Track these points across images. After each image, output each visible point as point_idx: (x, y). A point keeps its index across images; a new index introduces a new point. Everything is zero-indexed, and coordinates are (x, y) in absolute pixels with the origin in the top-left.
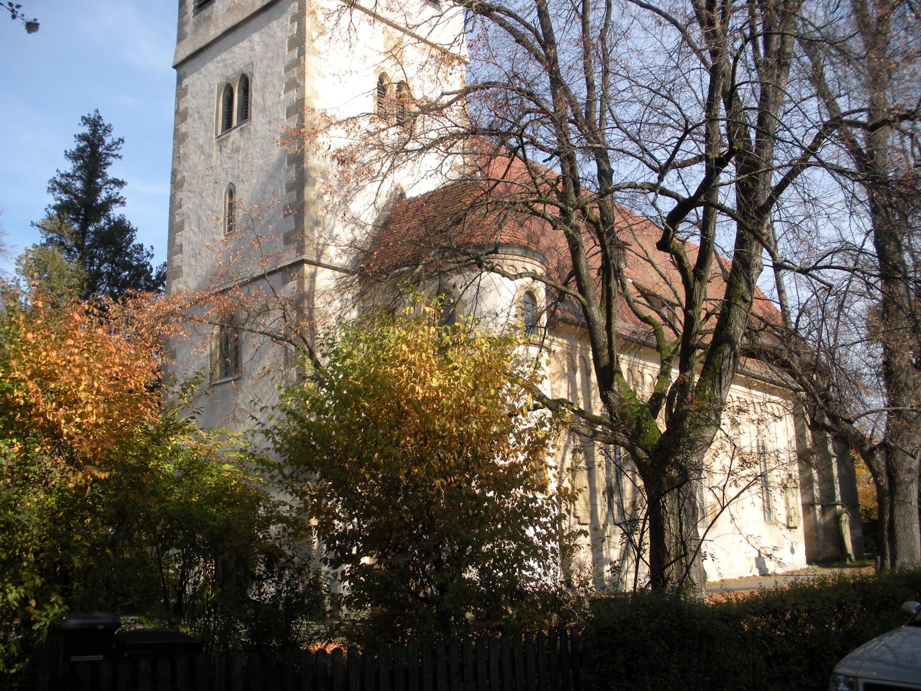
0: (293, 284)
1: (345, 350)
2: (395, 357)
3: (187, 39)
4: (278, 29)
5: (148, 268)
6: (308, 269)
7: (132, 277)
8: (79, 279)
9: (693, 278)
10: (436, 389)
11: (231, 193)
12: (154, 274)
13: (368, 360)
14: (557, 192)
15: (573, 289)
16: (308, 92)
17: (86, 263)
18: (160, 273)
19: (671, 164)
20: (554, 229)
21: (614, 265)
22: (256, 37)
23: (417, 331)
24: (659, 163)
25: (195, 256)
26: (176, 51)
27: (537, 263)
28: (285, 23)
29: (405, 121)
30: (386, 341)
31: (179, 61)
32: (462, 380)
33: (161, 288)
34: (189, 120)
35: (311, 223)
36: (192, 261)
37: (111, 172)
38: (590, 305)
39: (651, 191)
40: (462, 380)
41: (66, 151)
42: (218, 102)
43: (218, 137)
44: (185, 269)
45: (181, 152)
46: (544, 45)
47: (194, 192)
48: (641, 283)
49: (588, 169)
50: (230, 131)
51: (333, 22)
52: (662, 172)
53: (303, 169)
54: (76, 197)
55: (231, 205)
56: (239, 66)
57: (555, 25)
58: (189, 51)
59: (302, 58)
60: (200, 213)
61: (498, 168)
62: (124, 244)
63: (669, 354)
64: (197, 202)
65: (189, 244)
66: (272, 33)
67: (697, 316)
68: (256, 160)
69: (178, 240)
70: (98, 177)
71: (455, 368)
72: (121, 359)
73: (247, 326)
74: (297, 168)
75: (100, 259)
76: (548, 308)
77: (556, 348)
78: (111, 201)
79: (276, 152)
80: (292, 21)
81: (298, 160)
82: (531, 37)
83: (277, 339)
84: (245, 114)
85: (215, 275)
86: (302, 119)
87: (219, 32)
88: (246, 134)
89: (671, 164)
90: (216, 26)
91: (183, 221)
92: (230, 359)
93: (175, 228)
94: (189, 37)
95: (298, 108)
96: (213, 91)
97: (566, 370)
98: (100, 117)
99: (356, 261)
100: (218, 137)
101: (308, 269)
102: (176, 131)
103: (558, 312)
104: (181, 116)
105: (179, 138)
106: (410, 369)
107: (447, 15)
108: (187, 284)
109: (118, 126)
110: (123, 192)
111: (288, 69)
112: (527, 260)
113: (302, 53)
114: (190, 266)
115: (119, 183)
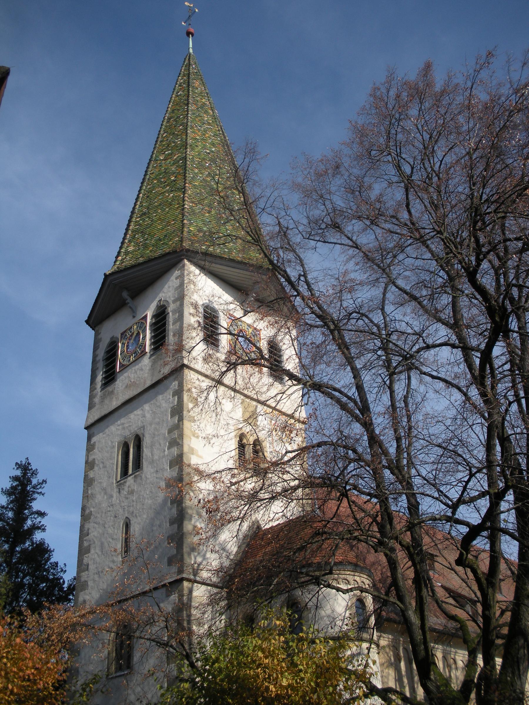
0: (174, 597)
1: (213, 656)
2: (254, 662)
3: (96, 408)
4: (164, 401)
5: (61, 581)
6: (186, 584)
7: (48, 588)
8: (6, 589)
9: (488, 582)
10: (286, 688)
11: (127, 525)
12: (66, 585)
13: (232, 663)
14: (378, 524)
15: (393, 599)
16: (186, 449)
17: (12, 576)
18: (71, 585)
19: (461, 501)
20: (376, 552)
21: (423, 577)
22: (147, 407)
23: (270, 640)
24: (451, 501)
25: (98, 573)
26: (87, 417)
27: (365, 576)
28: (168, 397)
29: (260, 472)
30: (246, 649)
31: (91, 421)
32: (306, 680)
33: (71, 597)
34: (96, 468)
35: (188, 549)
36: (96, 577)
37: (36, 506)
38: (407, 609)
39: (448, 521)
40: (306, 680)
41: (2, 489)
42: (118, 455)
43: (118, 482)
44: (90, 583)
45: (89, 492)
46: (362, 412)
47: (98, 523)
48: (447, 585)
49: (400, 506)
50: (126, 478)
51: (204, 398)
52: (454, 507)
53: (182, 508)
54: (8, 524)
55: (126, 539)
56: (134, 429)
57: (371, 398)
58: (96, 418)
59: (181, 423)
60: (103, 540)
61: (332, 505)
62: (43, 562)
63: (474, 646)
64: (101, 531)
65: (94, 563)
66: (158, 404)
67: (492, 615)
68: (146, 500)
69: (85, 561)
70: (26, 509)
71: (301, 671)
72: (33, 663)
73: (137, 634)
74: (178, 506)
75: (23, 573)
76: (375, 611)
77: (383, 642)
78: (35, 528)
79: (161, 496)
80: (173, 396)
81: (178, 501)
82: (351, 405)
83: (161, 644)
84: (138, 465)
85: (112, 593)
86: (181, 470)
87: (119, 403)
88: (139, 480)
89: (461, 501)
90: (117, 399)
91: (89, 546)
92: (123, 658)
93: (83, 551)
94: (97, 406)
95: (178, 461)
96: (114, 447)
97: (392, 659)
98: (29, 464)
99: (223, 578)
100: (118, 482)
101: (186, 584)
102: (86, 476)
103: (384, 613)
104: (90, 465)
105: (88, 482)
106: (265, 672)
107: (289, 392)
108: (90, 596)
109: (43, 470)
110: (44, 521)
111: (170, 431)
112: (356, 574)
113: (181, 419)
114: (94, 581)
115: (42, 514)
